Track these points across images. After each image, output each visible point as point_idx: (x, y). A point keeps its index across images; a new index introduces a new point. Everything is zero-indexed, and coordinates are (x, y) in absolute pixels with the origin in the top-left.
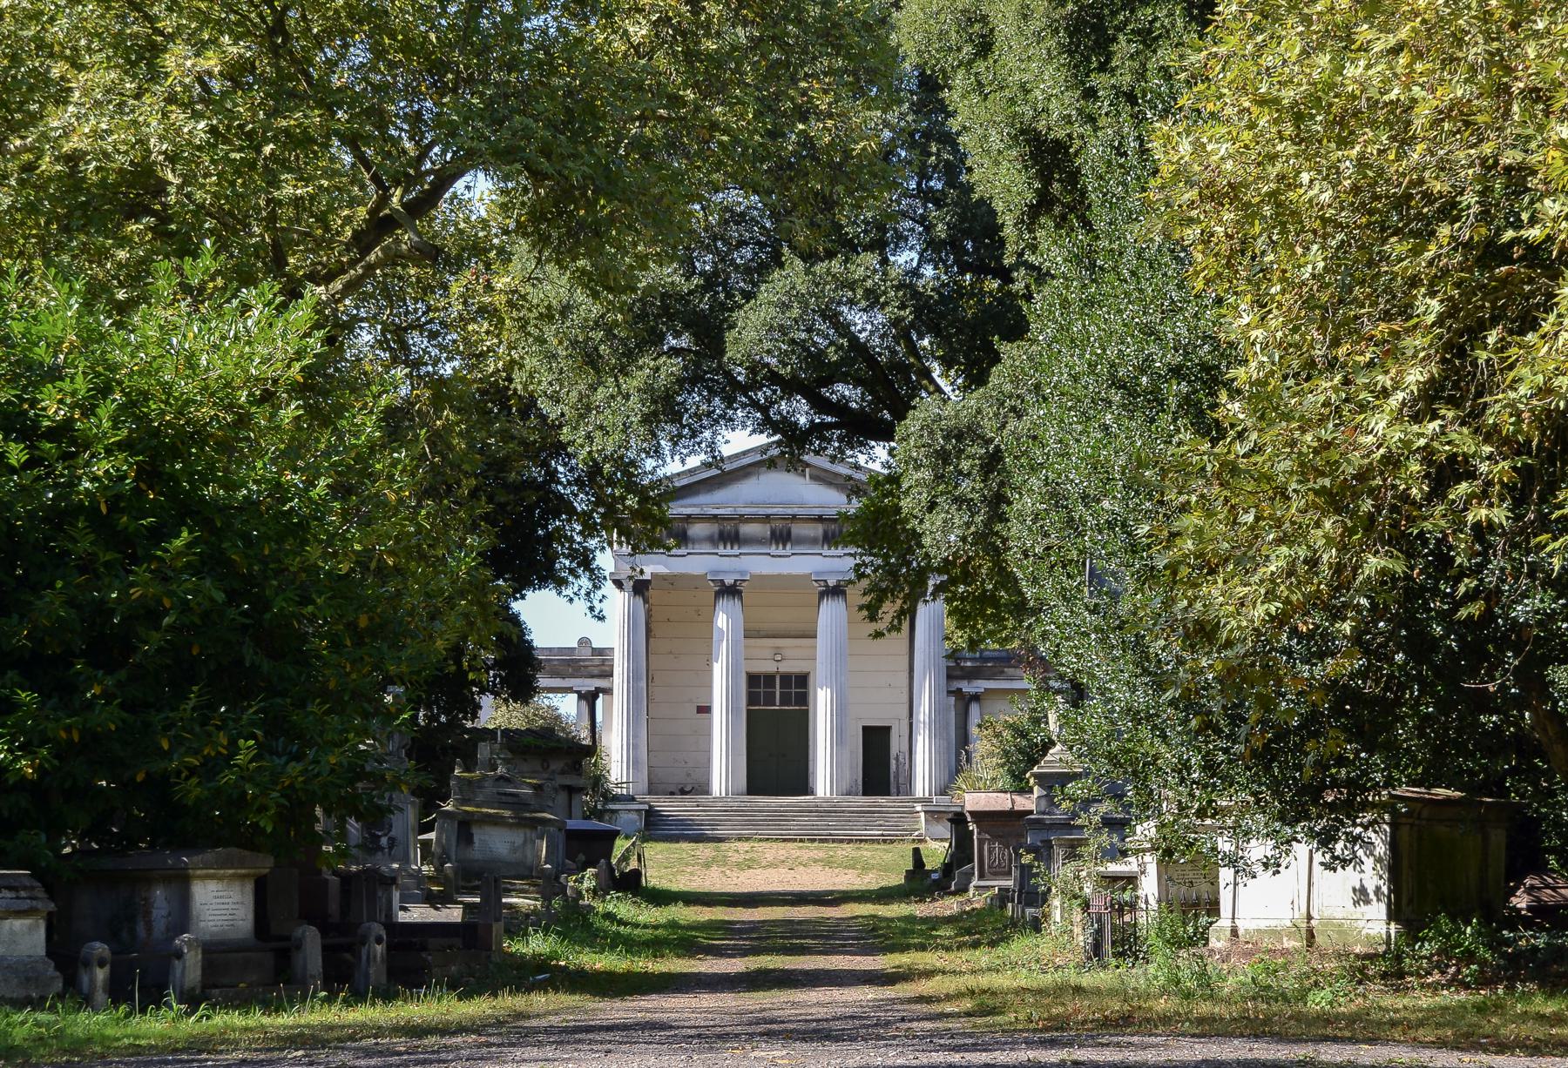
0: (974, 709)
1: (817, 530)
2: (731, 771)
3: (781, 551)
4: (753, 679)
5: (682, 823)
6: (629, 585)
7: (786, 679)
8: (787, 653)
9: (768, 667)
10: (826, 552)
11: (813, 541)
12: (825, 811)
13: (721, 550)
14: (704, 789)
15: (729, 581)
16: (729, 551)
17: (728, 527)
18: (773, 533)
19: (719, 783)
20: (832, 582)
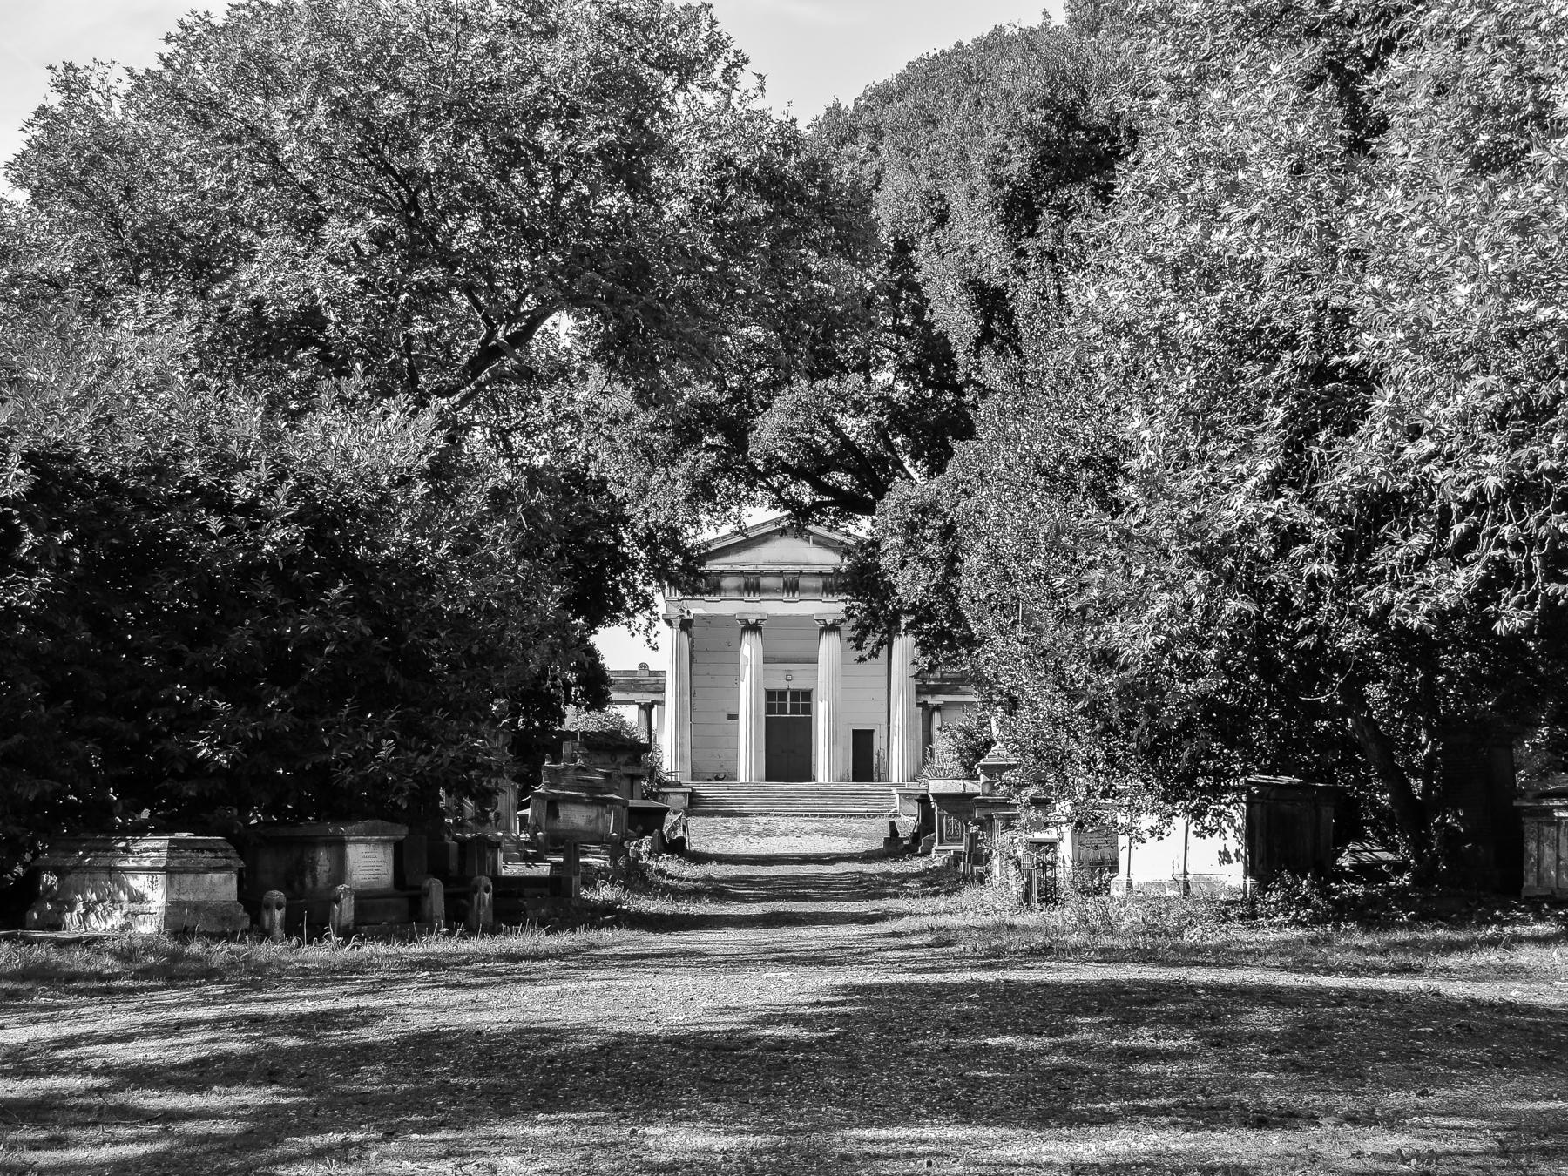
0: (937, 717)
1: (819, 582)
2: (753, 764)
3: (791, 598)
4: (770, 694)
5: (716, 802)
6: (677, 623)
7: (795, 694)
8: (795, 675)
9: (781, 685)
11: (816, 591)
12: (823, 793)
13: (746, 597)
14: (732, 777)
15: (752, 620)
16: (752, 598)
17: (752, 579)
18: (785, 584)
19: (743, 775)
20: (829, 621)
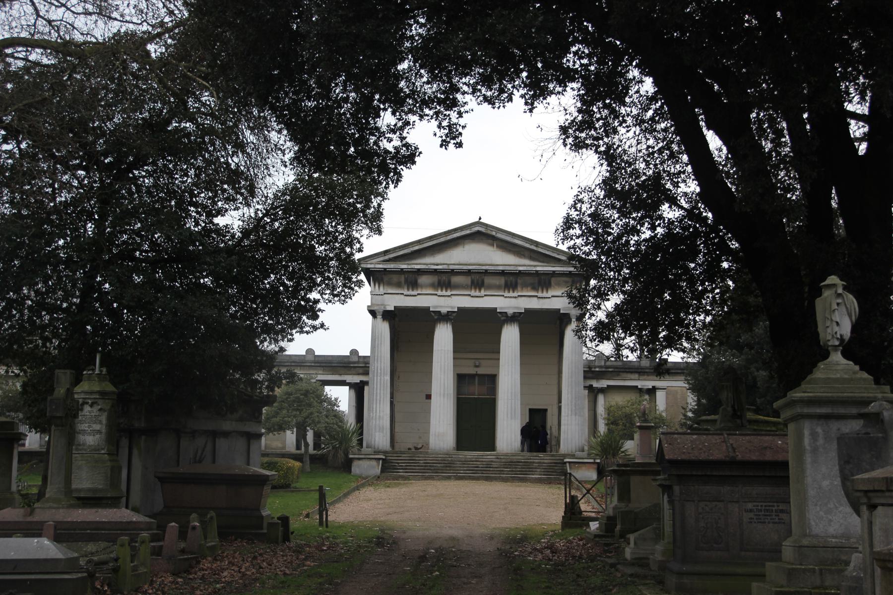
1: (501, 281)
10: (506, 294)
11: (498, 288)
16: (444, 293)
18: (473, 282)
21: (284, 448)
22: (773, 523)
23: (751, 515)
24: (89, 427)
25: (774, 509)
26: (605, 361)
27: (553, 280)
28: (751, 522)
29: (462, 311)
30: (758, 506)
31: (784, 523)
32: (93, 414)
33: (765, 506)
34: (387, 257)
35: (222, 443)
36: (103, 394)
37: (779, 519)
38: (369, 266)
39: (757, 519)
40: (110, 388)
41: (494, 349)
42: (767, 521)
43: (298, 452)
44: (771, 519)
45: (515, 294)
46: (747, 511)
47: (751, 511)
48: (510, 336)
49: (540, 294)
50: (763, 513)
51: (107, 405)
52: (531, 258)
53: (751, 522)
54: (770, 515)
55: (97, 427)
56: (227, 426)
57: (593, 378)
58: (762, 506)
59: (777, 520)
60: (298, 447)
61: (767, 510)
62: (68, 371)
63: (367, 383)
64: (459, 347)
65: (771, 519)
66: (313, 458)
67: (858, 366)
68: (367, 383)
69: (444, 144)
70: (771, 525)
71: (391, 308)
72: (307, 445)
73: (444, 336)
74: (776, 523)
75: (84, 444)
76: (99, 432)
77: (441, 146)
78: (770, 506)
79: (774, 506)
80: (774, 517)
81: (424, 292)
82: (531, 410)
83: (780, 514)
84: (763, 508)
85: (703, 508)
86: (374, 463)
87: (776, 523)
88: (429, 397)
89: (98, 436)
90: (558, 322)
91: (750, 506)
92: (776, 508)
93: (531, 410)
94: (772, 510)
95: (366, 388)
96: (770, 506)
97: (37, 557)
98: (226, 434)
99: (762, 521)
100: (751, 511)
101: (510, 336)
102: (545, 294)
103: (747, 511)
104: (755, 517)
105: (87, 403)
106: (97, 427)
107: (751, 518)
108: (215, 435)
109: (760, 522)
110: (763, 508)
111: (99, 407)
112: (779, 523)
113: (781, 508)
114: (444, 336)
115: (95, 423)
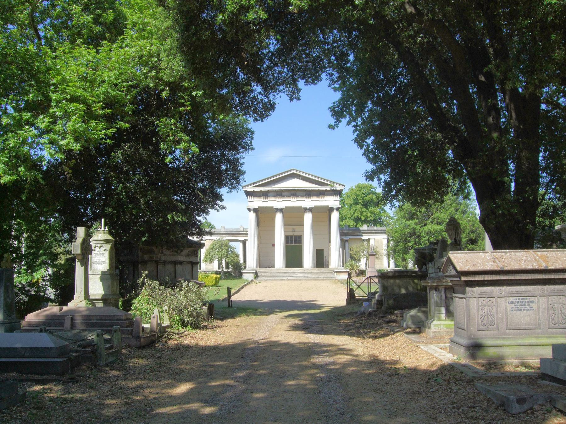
21: (213, 269)
22: (526, 310)
23: (513, 305)
24: (99, 260)
25: (527, 300)
26: (348, 227)
27: (326, 193)
28: (513, 310)
29: (287, 208)
30: (517, 299)
31: (533, 310)
32: (101, 253)
33: (521, 299)
34: (254, 185)
35: (179, 268)
36: (107, 242)
37: (530, 307)
38: (247, 189)
39: (516, 308)
40: (110, 238)
41: (301, 224)
42: (522, 309)
43: (219, 270)
44: (525, 308)
45: (310, 200)
46: (510, 303)
47: (512, 303)
48: (308, 218)
49: (320, 199)
50: (520, 304)
51: (108, 247)
52: (316, 184)
53: (513, 310)
54: (524, 305)
55: (103, 260)
56: (181, 258)
57: (343, 235)
58: (519, 299)
59: (529, 308)
60: (219, 268)
61: (523, 302)
62: (84, 228)
63: (247, 240)
64: (286, 224)
65: (525, 308)
66: (225, 273)
67: (103, 293)
68: (247, 240)
69: (291, 100)
70: (525, 311)
71: (257, 207)
72: (223, 267)
73: (279, 218)
74: (528, 310)
75: (97, 269)
76: (105, 262)
77: (291, 100)
78: (524, 299)
79: (526, 299)
80: (527, 306)
81: (271, 200)
82: (317, 250)
83: (531, 304)
84: (520, 300)
85: (481, 302)
86: (252, 274)
87: (528, 310)
88: (274, 245)
89: (104, 265)
90: (328, 212)
91: (511, 299)
92: (528, 300)
93: (317, 250)
94: (526, 302)
95: (247, 242)
96: (524, 299)
97: (38, 347)
98: (181, 263)
99: (519, 309)
100: (512, 303)
101: (308, 218)
102: (322, 199)
103: (510, 303)
104: (515, 307)
105: (98, 246)
106: (103, 260)
107: (512, 308)
108: (175, 263)
109: (519, 310)
110: (520, 300)
111: (104, 249)
112: (531, 310)
113: (531, 300)
114: (279, 218)
115: (102, 257)
